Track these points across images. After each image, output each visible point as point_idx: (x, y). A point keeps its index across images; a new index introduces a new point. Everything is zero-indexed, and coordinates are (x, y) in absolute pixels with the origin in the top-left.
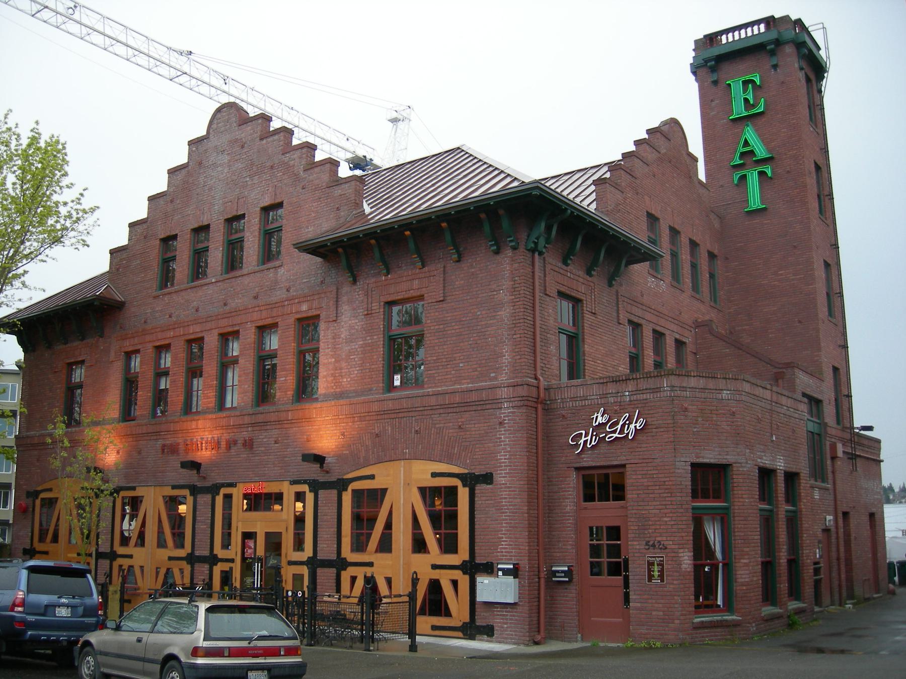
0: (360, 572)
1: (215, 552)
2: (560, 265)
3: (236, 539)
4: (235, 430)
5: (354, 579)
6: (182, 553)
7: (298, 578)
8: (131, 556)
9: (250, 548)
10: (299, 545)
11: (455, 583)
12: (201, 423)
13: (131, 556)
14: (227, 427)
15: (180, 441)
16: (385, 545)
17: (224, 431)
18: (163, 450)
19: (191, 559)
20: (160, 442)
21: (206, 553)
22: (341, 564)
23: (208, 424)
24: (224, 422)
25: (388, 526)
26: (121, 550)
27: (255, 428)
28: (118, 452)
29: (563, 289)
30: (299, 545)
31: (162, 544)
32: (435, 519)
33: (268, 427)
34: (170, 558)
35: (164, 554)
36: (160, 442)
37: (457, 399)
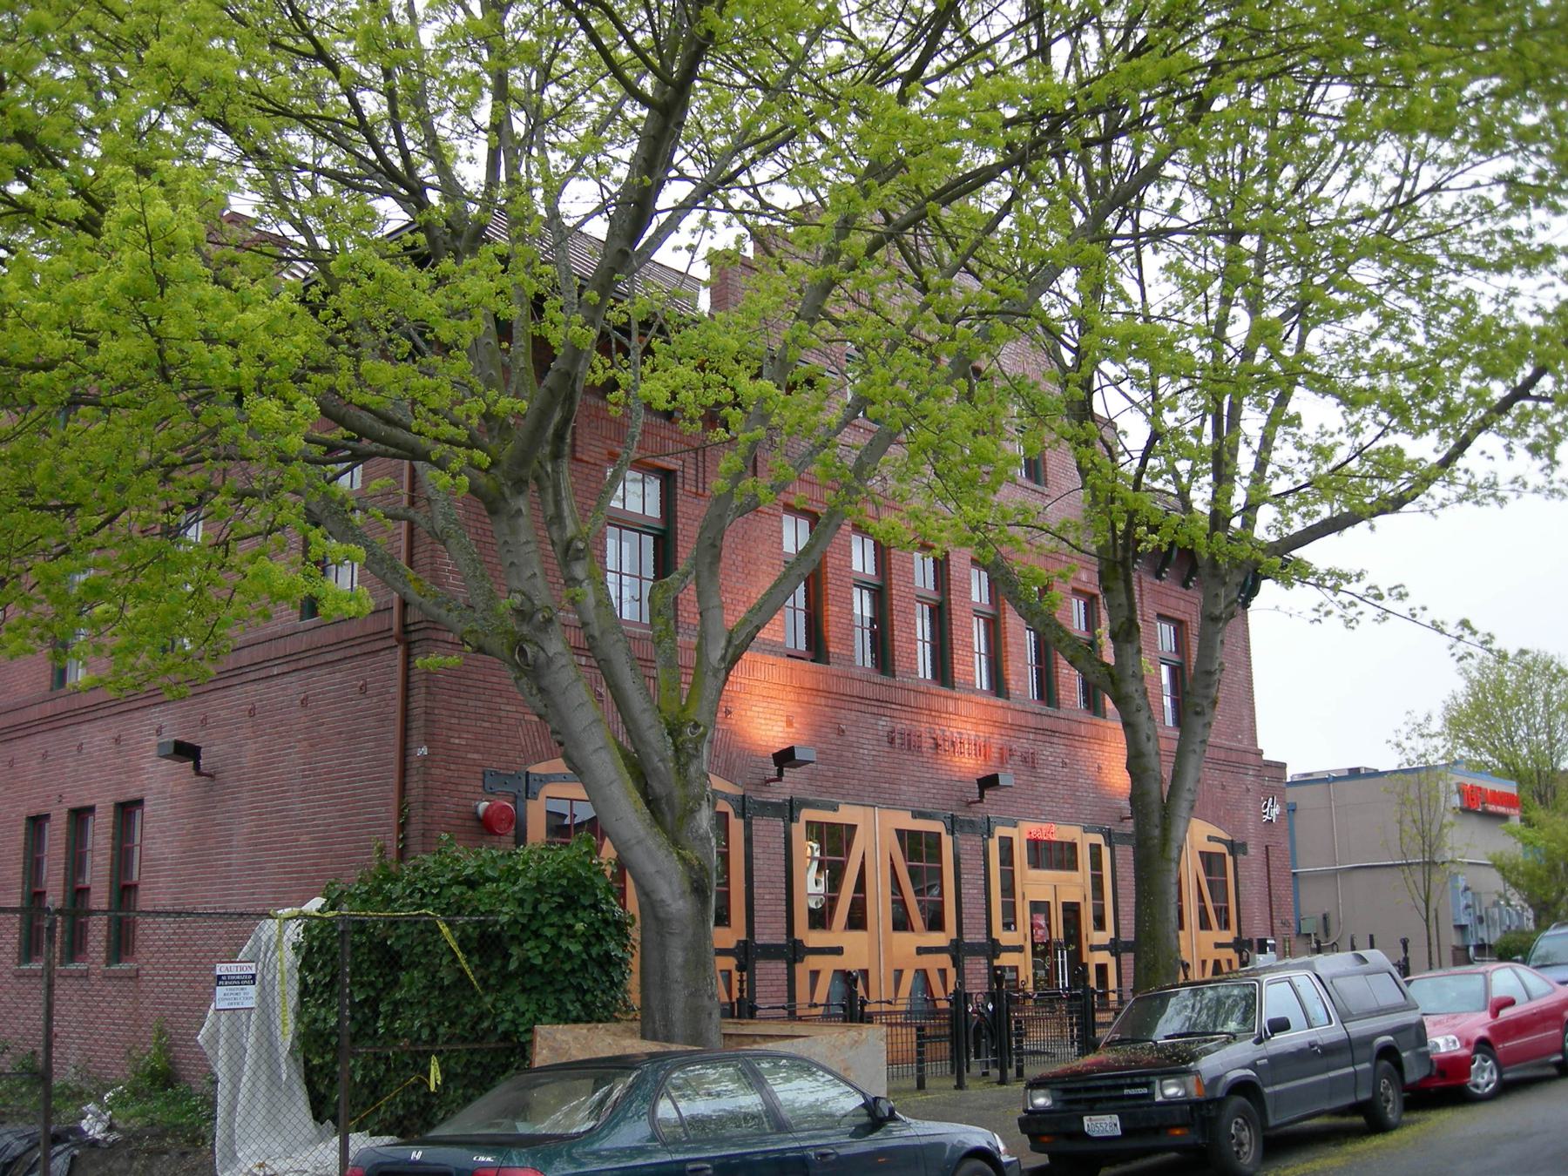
0: (826, 965)
1: (797, 936)
2: (1179, 589)
3: (1023, 913)
4: (1011, 733)
5: (815, 974)
6: (939, 939)
7: (1102, 969)
8: (838, 951)
9: (1040, 927)
10: (1100, 924)
11: (943, 972)
12: (964, 707)
13: (838, 951)
14: (1002, 725)
15: (923, 728)
16: (857, 920)
17: (996, 730)
18: (892, 741)
19: (958, 951)
20: (883, 724)
21: (980, 938)
22: (794, 952)
23: (975, 712)
24: (998, 715)
25: (861, 885)
26: (815, 939)
27: (1040, 737)
28: (789, 723)
29: (1163, 611)
30: (1100, 924)
31: (901, 923)
32: (914, 874)
33: (1055, 740)
34: (921, 951)
35: (907, 942)
36: (883, 724)
37: (1223, 756)
